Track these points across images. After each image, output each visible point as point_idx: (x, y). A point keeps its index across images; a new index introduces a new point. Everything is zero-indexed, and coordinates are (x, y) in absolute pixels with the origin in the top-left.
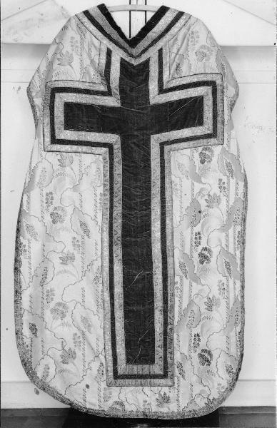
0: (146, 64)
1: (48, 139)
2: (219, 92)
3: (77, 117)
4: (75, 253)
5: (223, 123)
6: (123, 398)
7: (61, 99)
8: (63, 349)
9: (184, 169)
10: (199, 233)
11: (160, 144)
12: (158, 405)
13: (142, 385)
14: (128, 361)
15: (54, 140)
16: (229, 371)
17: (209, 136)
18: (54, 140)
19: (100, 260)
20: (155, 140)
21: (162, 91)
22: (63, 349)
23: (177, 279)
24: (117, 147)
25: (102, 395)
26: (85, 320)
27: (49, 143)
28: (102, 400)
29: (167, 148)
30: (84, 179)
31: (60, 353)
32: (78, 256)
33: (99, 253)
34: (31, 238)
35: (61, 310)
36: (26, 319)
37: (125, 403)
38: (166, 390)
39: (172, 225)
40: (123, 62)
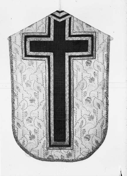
0: (64, 22)
1: (24, 55)
2: (94, 39)
3: (35, 45)
4: (35, 135)
5: (96, 50)
6: (53, 154)
7: (29, 39)
8: (30, 135)
9: (79, 68)
10: (86, 92)
11: (69, 56)
12: (67, 157)
13: (60, 149)
14: (55, 140)
15: (26, 55)
16: (97, 142)
17: (92, 40)
18: (26, 55)
19: (45, 101)
20: (67, 55)
21: (70, 36)
22: (30, 135)
23: (75, 109)
24: (52, 57)
25: (45, 153)
26: (38, 88)
27: (24, 56)
28: (45, 155)
29: (72, 34)
30: (37, 72)
31: (29, 136)
32: (36, 99)
33: (45, 98)
34: (18, 127)
35: (30, 120)
36: (16, 120)
37: (54, 156)
38: (70, 151)
39: (73, 89)
40: (54, 20)
